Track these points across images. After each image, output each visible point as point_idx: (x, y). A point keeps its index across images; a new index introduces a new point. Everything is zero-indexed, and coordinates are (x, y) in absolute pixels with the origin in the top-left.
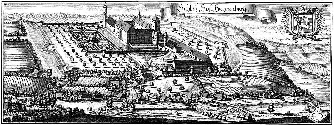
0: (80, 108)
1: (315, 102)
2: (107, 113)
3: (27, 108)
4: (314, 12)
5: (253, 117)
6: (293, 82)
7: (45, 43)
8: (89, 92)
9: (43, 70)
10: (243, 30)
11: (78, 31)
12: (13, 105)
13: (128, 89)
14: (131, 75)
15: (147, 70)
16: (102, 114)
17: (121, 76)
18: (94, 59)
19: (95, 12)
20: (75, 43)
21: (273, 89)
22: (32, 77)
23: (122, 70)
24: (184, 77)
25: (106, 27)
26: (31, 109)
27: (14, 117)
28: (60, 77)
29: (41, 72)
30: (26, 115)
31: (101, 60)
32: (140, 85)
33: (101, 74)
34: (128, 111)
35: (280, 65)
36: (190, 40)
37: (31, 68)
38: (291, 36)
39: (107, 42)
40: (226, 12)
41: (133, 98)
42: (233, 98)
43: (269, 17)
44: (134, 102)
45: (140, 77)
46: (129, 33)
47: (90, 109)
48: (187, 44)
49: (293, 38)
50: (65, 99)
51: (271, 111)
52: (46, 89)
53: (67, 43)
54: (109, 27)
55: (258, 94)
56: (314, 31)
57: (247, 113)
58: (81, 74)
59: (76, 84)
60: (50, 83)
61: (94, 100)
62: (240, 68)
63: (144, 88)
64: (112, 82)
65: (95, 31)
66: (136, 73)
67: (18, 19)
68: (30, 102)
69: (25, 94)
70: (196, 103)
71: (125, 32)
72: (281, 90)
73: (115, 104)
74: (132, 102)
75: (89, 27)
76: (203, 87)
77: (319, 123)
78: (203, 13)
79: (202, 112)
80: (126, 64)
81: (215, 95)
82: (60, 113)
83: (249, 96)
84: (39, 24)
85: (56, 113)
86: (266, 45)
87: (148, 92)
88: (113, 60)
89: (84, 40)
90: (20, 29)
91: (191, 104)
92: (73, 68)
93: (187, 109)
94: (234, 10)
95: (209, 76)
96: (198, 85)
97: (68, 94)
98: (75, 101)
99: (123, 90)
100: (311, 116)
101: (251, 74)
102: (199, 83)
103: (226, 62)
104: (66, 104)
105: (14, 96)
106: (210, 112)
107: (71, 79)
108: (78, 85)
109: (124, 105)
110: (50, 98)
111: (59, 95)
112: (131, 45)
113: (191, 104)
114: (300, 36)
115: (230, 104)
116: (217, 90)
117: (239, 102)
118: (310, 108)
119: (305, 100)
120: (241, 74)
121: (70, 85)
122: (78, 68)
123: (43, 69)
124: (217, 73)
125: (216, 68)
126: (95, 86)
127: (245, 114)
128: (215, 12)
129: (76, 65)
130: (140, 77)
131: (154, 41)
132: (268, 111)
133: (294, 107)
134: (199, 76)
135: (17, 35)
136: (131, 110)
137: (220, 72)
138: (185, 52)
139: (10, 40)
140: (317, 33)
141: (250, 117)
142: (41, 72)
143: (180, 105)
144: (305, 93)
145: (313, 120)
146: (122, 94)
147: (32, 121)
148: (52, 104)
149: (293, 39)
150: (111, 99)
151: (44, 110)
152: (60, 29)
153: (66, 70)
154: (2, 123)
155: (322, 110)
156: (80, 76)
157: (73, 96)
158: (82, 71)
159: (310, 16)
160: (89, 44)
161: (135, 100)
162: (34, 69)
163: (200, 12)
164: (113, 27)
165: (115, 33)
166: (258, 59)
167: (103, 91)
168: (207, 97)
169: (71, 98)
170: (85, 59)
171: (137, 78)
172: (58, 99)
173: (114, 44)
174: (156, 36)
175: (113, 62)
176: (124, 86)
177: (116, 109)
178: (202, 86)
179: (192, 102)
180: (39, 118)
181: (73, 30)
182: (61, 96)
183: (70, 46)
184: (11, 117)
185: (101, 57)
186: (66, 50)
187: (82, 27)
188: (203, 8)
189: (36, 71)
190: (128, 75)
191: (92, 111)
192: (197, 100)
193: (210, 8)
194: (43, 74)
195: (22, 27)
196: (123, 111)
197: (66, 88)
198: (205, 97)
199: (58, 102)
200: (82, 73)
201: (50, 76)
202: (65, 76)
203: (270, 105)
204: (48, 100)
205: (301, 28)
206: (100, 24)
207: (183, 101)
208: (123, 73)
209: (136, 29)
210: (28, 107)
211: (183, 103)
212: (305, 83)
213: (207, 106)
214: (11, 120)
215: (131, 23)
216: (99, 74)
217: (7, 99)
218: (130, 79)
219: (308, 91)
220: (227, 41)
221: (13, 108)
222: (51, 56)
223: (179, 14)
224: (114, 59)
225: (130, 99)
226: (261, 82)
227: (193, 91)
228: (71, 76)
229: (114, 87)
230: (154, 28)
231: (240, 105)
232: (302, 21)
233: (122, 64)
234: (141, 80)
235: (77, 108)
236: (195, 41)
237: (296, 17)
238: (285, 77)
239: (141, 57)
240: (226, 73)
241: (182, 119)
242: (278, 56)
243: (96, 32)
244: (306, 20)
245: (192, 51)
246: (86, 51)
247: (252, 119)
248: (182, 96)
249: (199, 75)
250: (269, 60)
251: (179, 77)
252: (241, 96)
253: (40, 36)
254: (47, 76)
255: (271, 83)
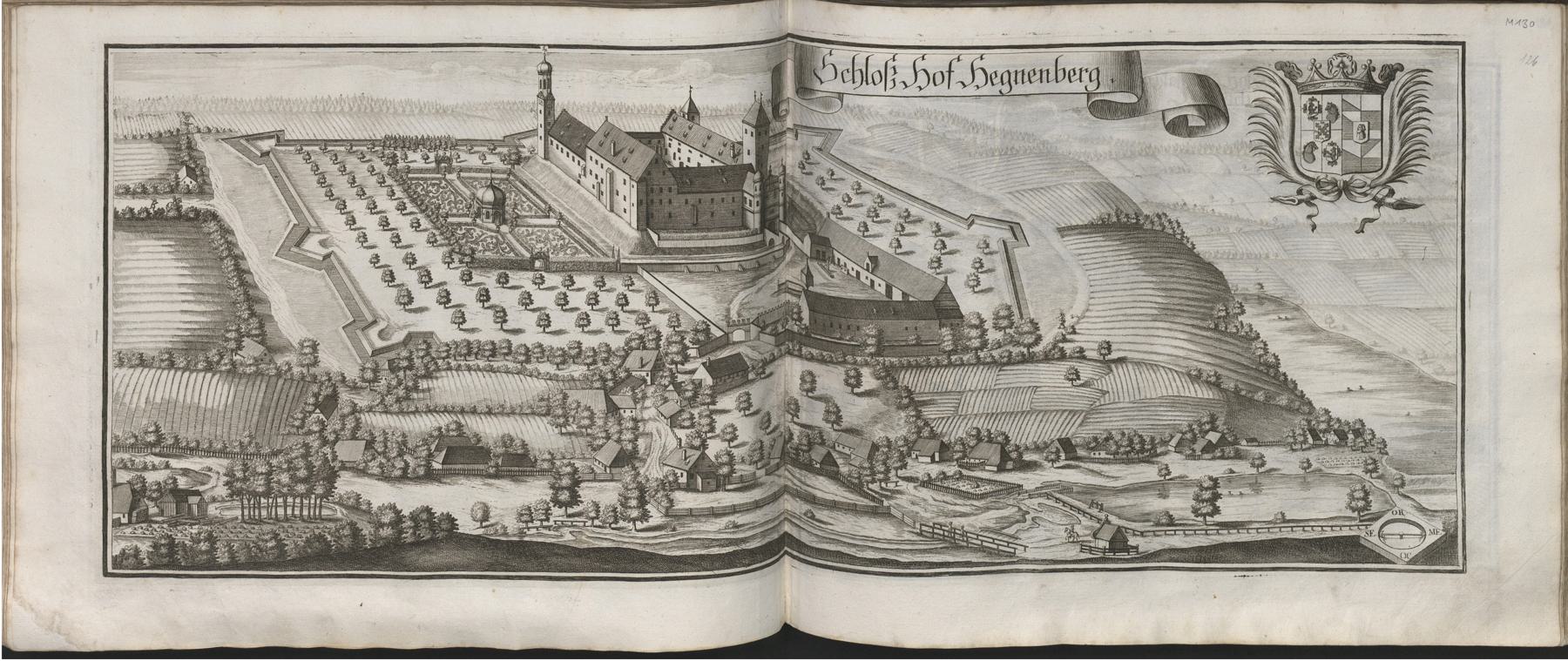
0: (438, 510)
1: (1395, 471)
2: (552, 533)
3: (212, 510)
4: (1386, 85)
5: (1132, 541)
6: (1299, 388)
7: (291, 225)
8: (479, 441)
9: (282, 343)
10: (1091, 164)
11: (428, 171)
12: (150, 498)
13: (641, 430)
14: (658, 367)
15: (726, 341)
16: (532, 536)
17: (612, 371)
18: (499, 296)
19: (505, 92)
20: (416, 226)
21: (1213, 420)
22: (233, 372)
23: (617, 342)
24: (841, 370)
25: (546, 158)
26: (228, 514)
27: (156, 546)
28: (352, 373)
29: (272, 350)
30: (206, 540)
31: (527, 300)
32: (696, 412)
33: (528, 361)
34: (645, 525)
35: (1243, 312)
36: (864, 210)
37: (228, 335)
38: (1291, 189)
39: (553, 221)
40: (1018, 89)
41: (666, 469)
42: (1046, 459)
43: (1198, 107)
44: (669, 486)
45: (696, 376)
46: (645, 183)
47: (479, 515)
48: (852, 227)
49: (1300, 197)
50: (374, 468)
51: (1204, 511)
52: (293, 426)
53: (385, 224)
54: (562, 155)
55: (1153, 439)
56: (1388, 165)
57: (1108, 522)
58: (444, 359)
59: (421, 406)
60: (311, 400)
61: (496, 476)
62: (1076, 327)
63: (713, 421)
64: (574, 396)
65: (504, 172)
66: (678, 358)
67: (173, 123)
68: (227, 484)
69: (203, 450)
70: (891, 486)
71: (627, 178)
72: (1249, 422)
73: (588, 493)
74: (662, 484)
75: (476, 156)
76: (918, 416)
77: (1408, 563)
78: (922, 93)
79: (918, 526)
80: (634, 317)
81: (973, 448)
82: (356, 532)
83: (1114, 448)
84: (266, 145)
85: (337, 530)
86: (1183, 227)
87: (728, 437)
88: (577, 300)
89: (455, 211)
90: (183, 163)
91: (870, 486)
92: (410, 336)
93: (853, 509)
94: (1052, 76)
95: (946, 366)
96: (900, 407)
97: (386, 447)
98: (418, 479)
99: (620, 432)
100: (1376, 533)
101: (1121, 354)
102: (902, 398)
103: (1018, 303)
104: (379, 494)
105: (155, 455)
106: (949, 520)
107: (400, 383)
108: (428, 407)
109: (627, 499)
110: (309, 467)
111: (349, 451)
112: (654, 237)
113: (870, 486)
114: (1329, 188)
115: (1033, 487)
116: (980, 427)
117: (1072, 476)
118: (1371, 498)
119: (1348, 463)
120: (1081, 355)
121: (395, 408)
122: (427, 337)
123: (280, 337)
124: (982, 354)
125: (974, 333)
126: (502, 414)
127: (1098, 526)
128: (971, 90)
129: (423, 323)
130: (696, 376)
131: (753, 213)
132: (1196, 511)
133: (1305, 494)
134: (902, 367)
135: (172, 191)
136: (656, 518)
137: (992, 349)
138: (843, 260)
139: (139, 213)
140: (1400, 174)
141: (1119, 543)
142: (272, 350)
143: (825, 488)
144: (1351, 436)
145: (1383, 553)
146: (618, 447)
147: (233, 564)
148: (319, 490)
149: (1300, 202)
150: (569, 469)
151: (287, 519)
152: (352, 162)
153: (379, 344)
154: (106, 574)
155: (1422, 510)
156: (438, 369)
157: (408, 458)
158: (447, 345)
159: (1371, 102)
160: (478, 230)
161: (675, 474)
162: (243, 336)
163: (907, 92)
164: (577, 158)
165: (589, 181)
166: (1152, 285)
167: (539, 435)
168: (937, 459)
169: (399, 464)
170: (464, 295)
171: (680, 378)
172: (344, 467)
173: (584, 231)
174: (758, 192)
175: (576, 309)
176: (627, 414)
177: (593, 514)
178: (916, 409)
179: (873, 481)
180: (261, 551)
181: (409, 170)
182: (359, 457)
183: (396, 240)
184: (145, 547)
185: (530, 287)
186: (377, 256)
187: (448, 154)
188: (921, 75)
189: (252, 349)
190: (643, 366)
191: (492, 521)
192: (893, 472)
193: (950, 72)
194: (280, 360)
195: (191, 158)
196: (621, 524)
197: (378, 421)
198: (929, 460)
199: (346, 484)
200: (444, 355)
201: (313, 370)
202: (376, 371)
203: (1202, 488)
204: (302, 473)
205: (1335, 154)
206: (524, 142)
207: (838, 473)
208: (624, 358)
209: (676, 164)
210: (217, 505)
211: (835, 476)
212: (1349, 390)
213: (935, 496)
214: (146, 561)
215: (655, 141)
216: (521, 363)
217: (125, 467)
218: (652, 384)
219: (1363, 425)
220: (1019, 210)
221: (153, 510)
222: (317, 280)
223: (820, 94)
224: (583, 295)
225: (653, 471)
226: (1163, 386)
227: (878, 434)
228: (400, 369)
229: (584, 418)
230: (749, 159)
231: (1075, 489)
232: (1337, 124)
233: (617, 318)
234: (698, 385)
235: (428, 510)
236: (884, 214)
237: (1311, 105)
238: (1268, 366)
239: (700, 287)
240: (1015, 350)
241: (832, 547)
242: (1239, 277)
243: (505, 176)
244: (1354, 116)
245: (874, 259)
246: (467, 259)
247: (1127, 549)
248: (834, 447)
249: (904, 361)
250: (1201, 293)
251: (824, 367)
252: (1081, 452)
253: (267, 193)
254: (296, 370)
255: (1205, 393)
